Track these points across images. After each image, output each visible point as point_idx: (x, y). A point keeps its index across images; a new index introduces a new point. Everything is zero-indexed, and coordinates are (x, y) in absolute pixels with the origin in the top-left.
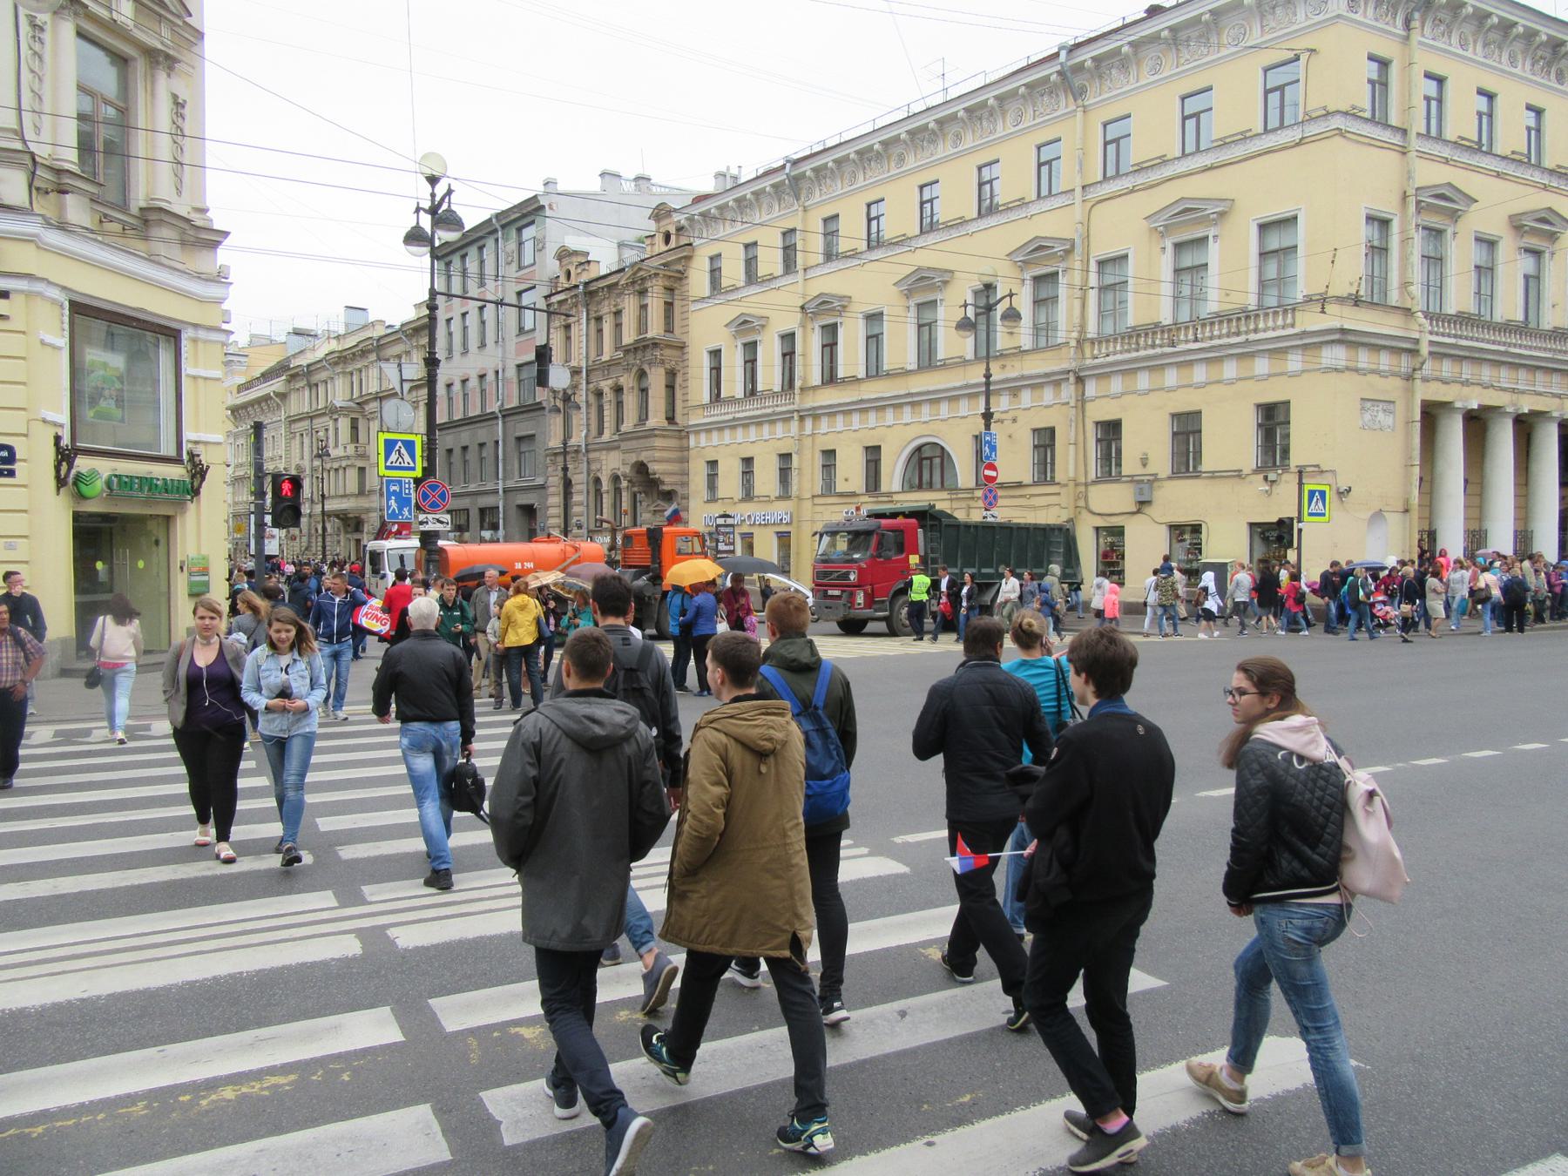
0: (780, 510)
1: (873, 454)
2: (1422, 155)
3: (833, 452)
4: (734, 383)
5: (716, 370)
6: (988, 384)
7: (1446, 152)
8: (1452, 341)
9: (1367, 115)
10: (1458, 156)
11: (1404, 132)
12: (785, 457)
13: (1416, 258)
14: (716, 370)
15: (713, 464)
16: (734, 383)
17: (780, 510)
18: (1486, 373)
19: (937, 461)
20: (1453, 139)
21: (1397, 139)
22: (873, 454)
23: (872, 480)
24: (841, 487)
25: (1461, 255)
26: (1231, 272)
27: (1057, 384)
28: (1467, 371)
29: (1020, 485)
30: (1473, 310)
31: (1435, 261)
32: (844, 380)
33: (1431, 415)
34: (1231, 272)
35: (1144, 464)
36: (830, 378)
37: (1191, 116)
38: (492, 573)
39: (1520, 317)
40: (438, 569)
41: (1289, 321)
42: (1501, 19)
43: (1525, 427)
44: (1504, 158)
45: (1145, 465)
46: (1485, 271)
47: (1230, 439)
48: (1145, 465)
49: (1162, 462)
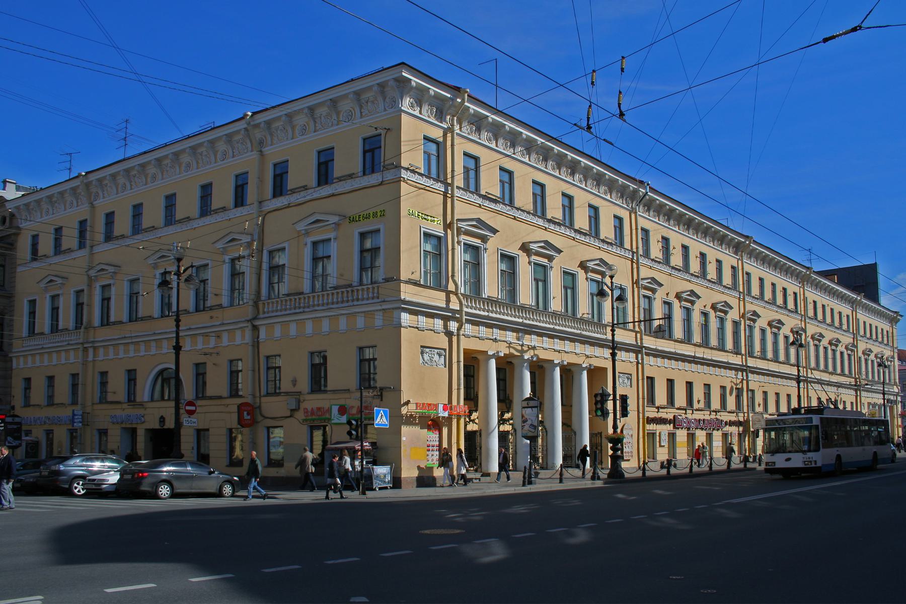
0: (126, 411)
1: (132, 377)
2: (462, 200)
3: (709, 385)
4: (44, 322)
5: (32, 313)
6: (177, 333)
7: (480, 201)
8: (552, 326)
12: (75, 376)
14: (32, 313)
15: (28, 380)
16: (44, 322)
17: (126, 411)
19: (173, 382)
22: (132, 377)
24: (110, 397)
27: (206, 335)
29: (220, 398)
32: (114, 323)
33: (472, 365)
36: (106, 321)
37: (369, 151)
38: (872, 443)
40: (808, 440)
45: (294, 385)
48: (294, 385)
49: (304, 384)
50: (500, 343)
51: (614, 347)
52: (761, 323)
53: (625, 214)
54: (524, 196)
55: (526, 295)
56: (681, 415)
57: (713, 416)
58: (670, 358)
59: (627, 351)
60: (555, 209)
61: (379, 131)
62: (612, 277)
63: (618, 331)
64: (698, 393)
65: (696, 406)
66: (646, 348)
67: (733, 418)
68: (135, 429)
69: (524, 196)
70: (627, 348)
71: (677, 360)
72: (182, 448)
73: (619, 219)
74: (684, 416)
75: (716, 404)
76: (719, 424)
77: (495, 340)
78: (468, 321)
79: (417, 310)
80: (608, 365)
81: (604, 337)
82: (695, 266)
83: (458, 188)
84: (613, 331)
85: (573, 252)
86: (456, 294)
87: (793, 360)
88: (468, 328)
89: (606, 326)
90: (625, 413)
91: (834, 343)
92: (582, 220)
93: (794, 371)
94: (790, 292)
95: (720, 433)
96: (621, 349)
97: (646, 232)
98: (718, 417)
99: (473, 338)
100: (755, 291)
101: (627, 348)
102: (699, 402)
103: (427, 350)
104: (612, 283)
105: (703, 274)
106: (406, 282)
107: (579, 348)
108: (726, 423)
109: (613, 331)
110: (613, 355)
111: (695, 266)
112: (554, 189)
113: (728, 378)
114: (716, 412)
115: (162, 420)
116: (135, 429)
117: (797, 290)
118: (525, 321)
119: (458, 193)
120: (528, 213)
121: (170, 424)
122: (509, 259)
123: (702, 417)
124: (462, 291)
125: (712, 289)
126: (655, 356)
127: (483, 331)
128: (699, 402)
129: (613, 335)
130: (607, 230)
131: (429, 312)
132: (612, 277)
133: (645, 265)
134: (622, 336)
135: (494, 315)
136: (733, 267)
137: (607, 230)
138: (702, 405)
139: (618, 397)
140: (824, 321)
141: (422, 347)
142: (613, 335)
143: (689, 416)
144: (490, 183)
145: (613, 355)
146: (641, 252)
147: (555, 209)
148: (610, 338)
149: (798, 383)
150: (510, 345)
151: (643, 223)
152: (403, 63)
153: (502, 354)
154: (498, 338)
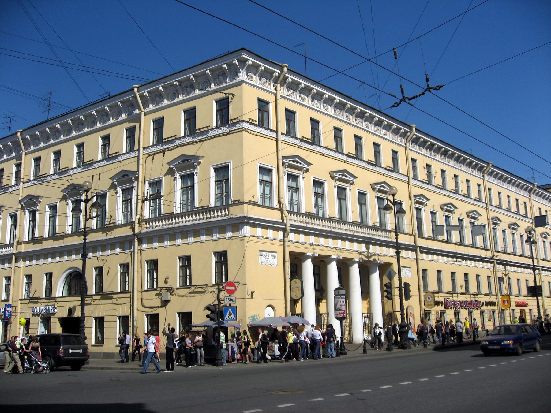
2: (284, 142)
8: (305, 225)
9: (257, 123)
10: (368, 166)
11: (276, 132)
13: (286, 188)
18: (322, 241)
20: (347, 153)
21: (274, 135)
23: (48, 290)
25: (352, 197)
26: (206, 191)
28: (312, 239)
30: (314, 211)
31: (293, 190)
33: (296, 263)
34: (206, 191)
35: (166, 282)
39: (471, 243)
41: (227, 212)
42: (370, 114)
43: (320, 264)
44: (435, 186)
46: (362, 203)
47: (205, 271)
50: (353, 250)
51: (398, 247)
52: (503, 225)
53: (481, 182)
54: (327, 138)
55: (332, 208)
56: (450, 298)
57: (473, 298)
58: (438, 255)
59: (407, 250)
60: (349, 146)
61: (227, 95)
62: (393, 195)
63: (400, 236)
64: (460, 280)
65: (459, 290)
66: (420, 247)
67: (487, 299)
68: (157, 316)
69: (327, 138)
70: (408, 248)
71: (443, 256)
72: (86, 331)
73: (394, 152)
74: (451, 299)
75: (473, 289)
76: (476, 305)
77: (312, 244)
78: (292, 231)
79: (255, 223)
80: (394, 261)
81: (390, 240)
82: (450, 185)
83: (282, 134)
84: (397, 235)
85: (365, 178)
86: (537, 259)
87: (528, 253)
88: (292, 236)
89: (389, 232)
90: (408, 297)
91: (513, 226)
92: (368, 154)
93: (530, 262)
94: (521, 202)
95: (478, 312)
96: (402, 249)
97: (414, 161)
98: (477, 299)
99: (299, 243)
100: (495, 202)
101: (408, 248)
102: (461, 287)
103: (264, 253)
104: (394, 199)
105: (358, 156)
106: (248, 203)
107: (331, 242)
108: (483, 303)
109: (397, 235)
110: (398, 253)
111: (450, 185)
112: (436, 168)
113: (485, 269)
114: (474, 295)
115: (71, 311)
116: (157, 316)
117: (481, 182)
118: (333, 230)
119: (281, 137)
120: (332, 150)
121: (77, 314)
122: (318, 184)
123: (464, 299)
124: (288, 209)
125: (465, 202)
126: (427, 253)
127: (302, 238)
128: (461, 287)
129: (397, 239)
130: (386, 160)
131: (265, 225)
132: (393, 195)
133: (415, 185)
134: (403, 239)
135: (310, 226)
136: (479, 185)
137: (386, 160)
138: (464, 290)
139: (403, 286)
140: (518, 213)
141: (260, 251)
142: (397, 239)
143: (455, 299)
144: (303, 129)
145: (398, 253)
146: (411, 176)
147: (349, 146)
148: (395, 241)
149: (534, 271)
150: (361, 253)
151: (488, 185)
152: (243, 49)
153: (341, 258)
154: (314, 243)
